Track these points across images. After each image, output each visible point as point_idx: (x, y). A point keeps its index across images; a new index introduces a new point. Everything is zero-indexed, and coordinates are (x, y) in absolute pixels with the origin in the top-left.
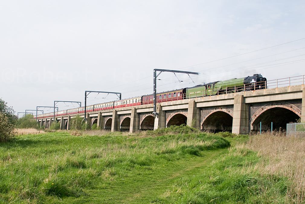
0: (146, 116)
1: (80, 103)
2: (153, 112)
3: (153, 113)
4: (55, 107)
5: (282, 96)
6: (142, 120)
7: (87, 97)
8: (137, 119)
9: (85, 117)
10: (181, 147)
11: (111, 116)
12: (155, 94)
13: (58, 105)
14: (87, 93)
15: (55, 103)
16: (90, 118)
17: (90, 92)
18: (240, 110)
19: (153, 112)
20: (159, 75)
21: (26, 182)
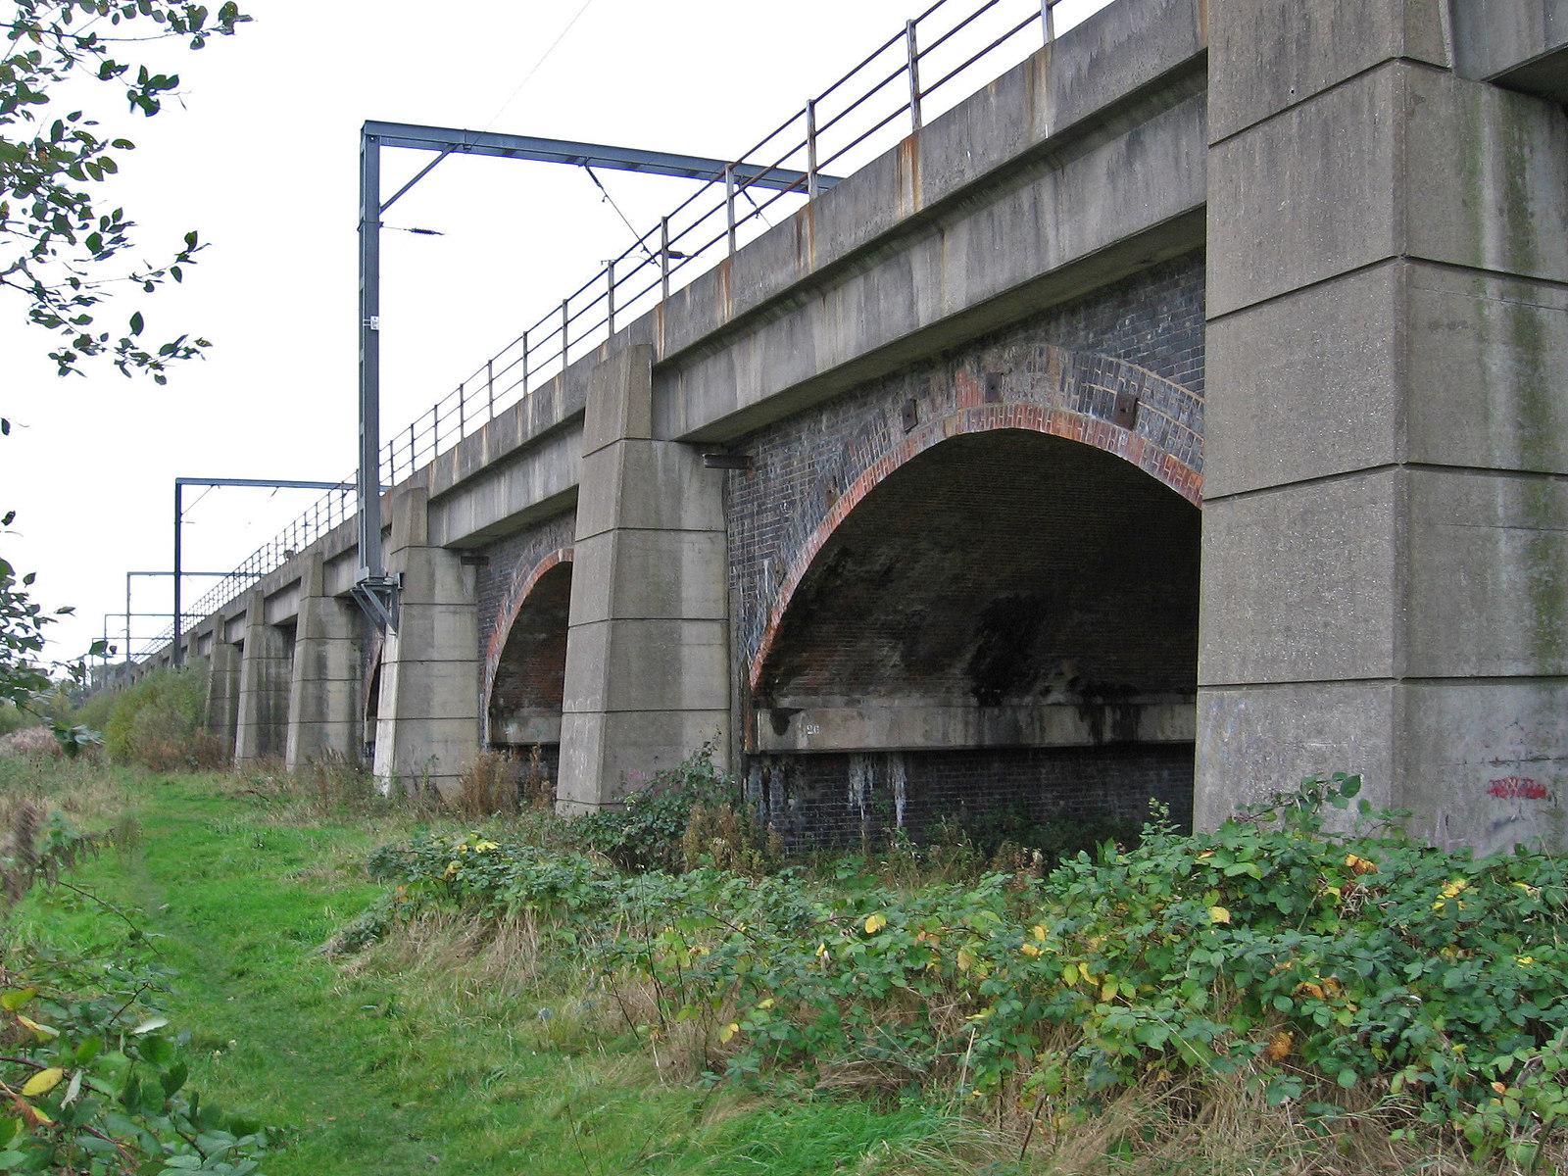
5: (945, 735)
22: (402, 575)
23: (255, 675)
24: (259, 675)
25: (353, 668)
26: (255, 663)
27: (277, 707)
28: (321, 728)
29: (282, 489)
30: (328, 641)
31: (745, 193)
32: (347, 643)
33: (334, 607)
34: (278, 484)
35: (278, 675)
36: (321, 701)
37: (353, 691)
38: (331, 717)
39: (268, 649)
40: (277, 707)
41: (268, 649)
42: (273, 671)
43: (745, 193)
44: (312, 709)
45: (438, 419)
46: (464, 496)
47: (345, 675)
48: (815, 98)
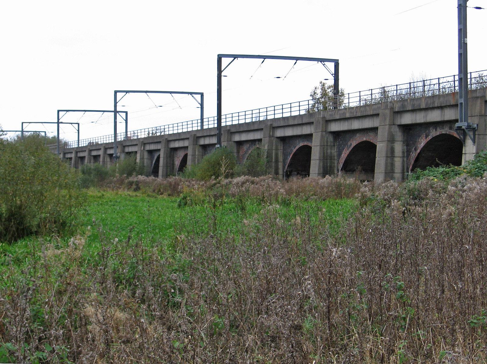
0: (430, 138)
1: (198, 97)
2: (457, 121)
3: (457, 125)
4: (116, 112)
5: (204, 143)
6: (416, 150)
7: (223, 74)
8: (399, 148)
9: (219, 142)
10: (352, 200)
11: (309, 137)
12: (312, 100)
13: (125, 103)
14: (225, 61)
15: (77, 123)
16: (235, 145)
17: (235, 57)
18: (319, 144)
19: (457, 121)
20: (194, 98)
21: (99, 288)
22: (477, 125)
23: (322, 153)
24: (324, 153)
25: (403, 152)
26: (322, 148)
27: (331, 167)
28: (392, 175)
29: (267, 60)
30: (395, 142)
31: (62, 123)
32: (402, 143)
33: (397, 129)
34: (265, 57)
35: (331, 153)
36: (392, 165)
37: (403, 161)
38: (396, 171)
39: (327, 142)
40: (331, 167)
41: (327, 142)
42: (329, 151)
43: (62, 123)
44: (389, 168)
45: (440, 82)
46: (430, 111)
47: (401, 155)
48: (63, 122)
